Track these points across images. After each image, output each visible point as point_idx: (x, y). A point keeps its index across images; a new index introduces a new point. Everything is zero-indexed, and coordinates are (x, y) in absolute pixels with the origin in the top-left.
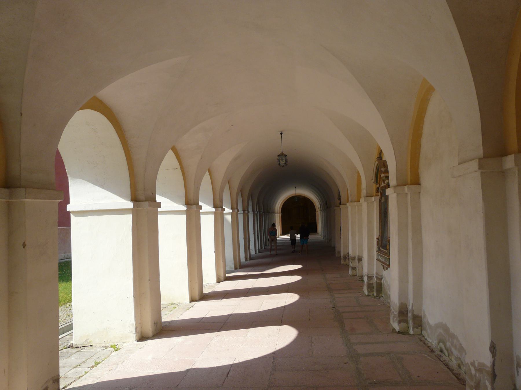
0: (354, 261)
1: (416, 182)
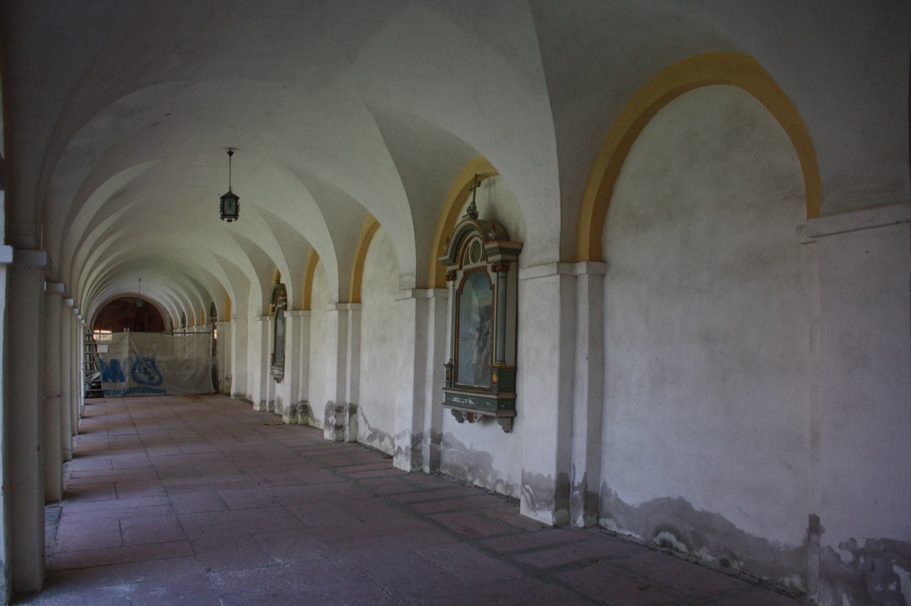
0: (340, 413)
1: (357, 300)
